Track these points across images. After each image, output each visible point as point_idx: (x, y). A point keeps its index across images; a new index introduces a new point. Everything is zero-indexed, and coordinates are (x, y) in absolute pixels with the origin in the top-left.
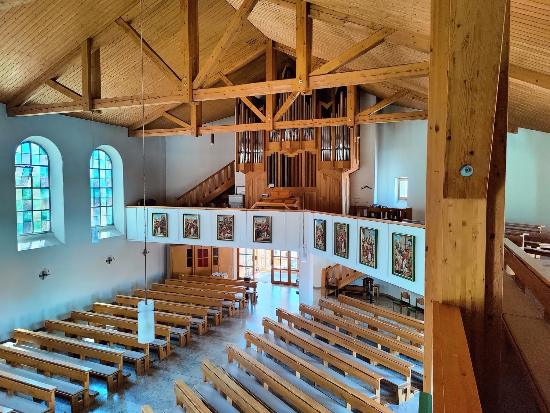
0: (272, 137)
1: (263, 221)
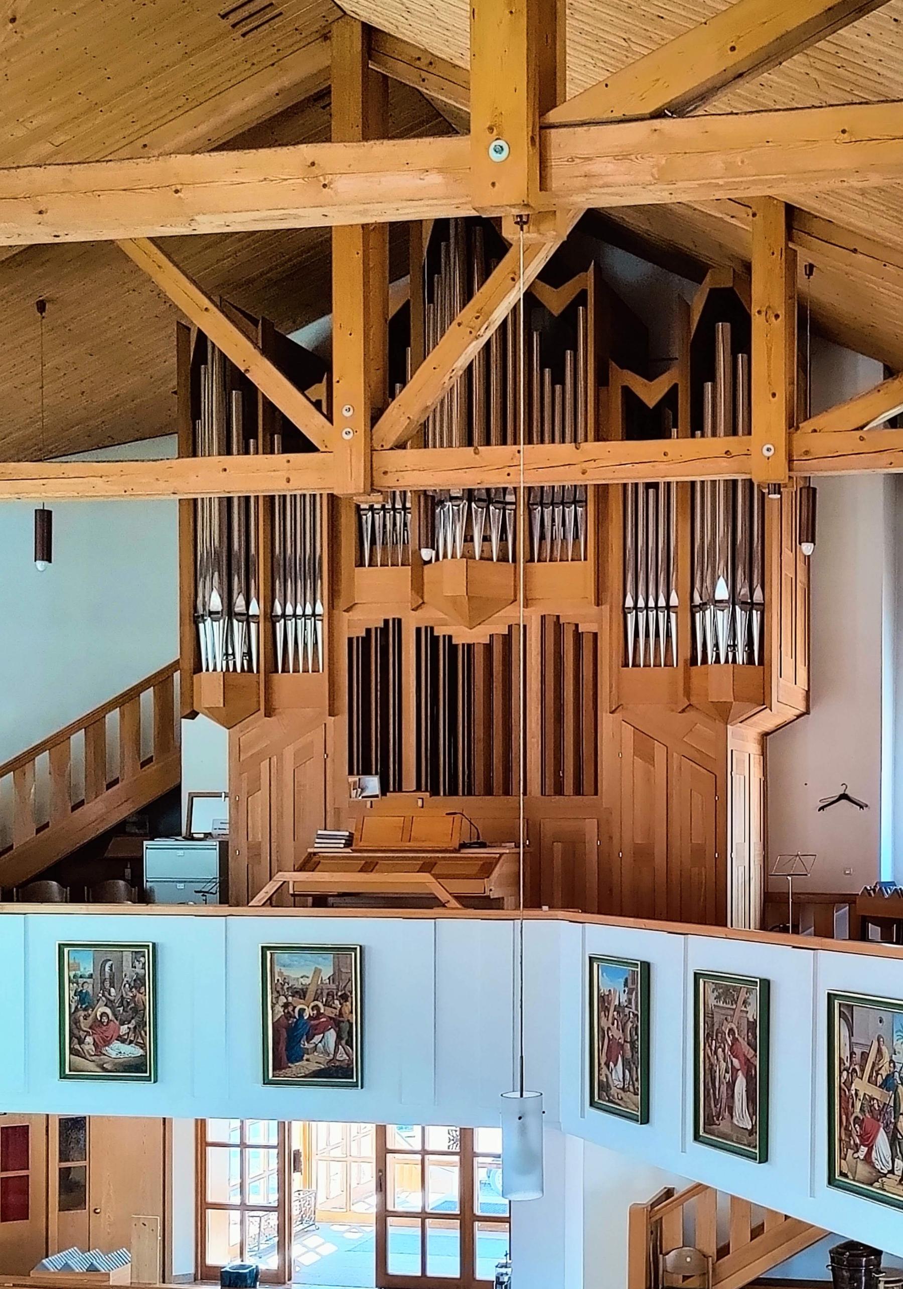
1: (317, 972)
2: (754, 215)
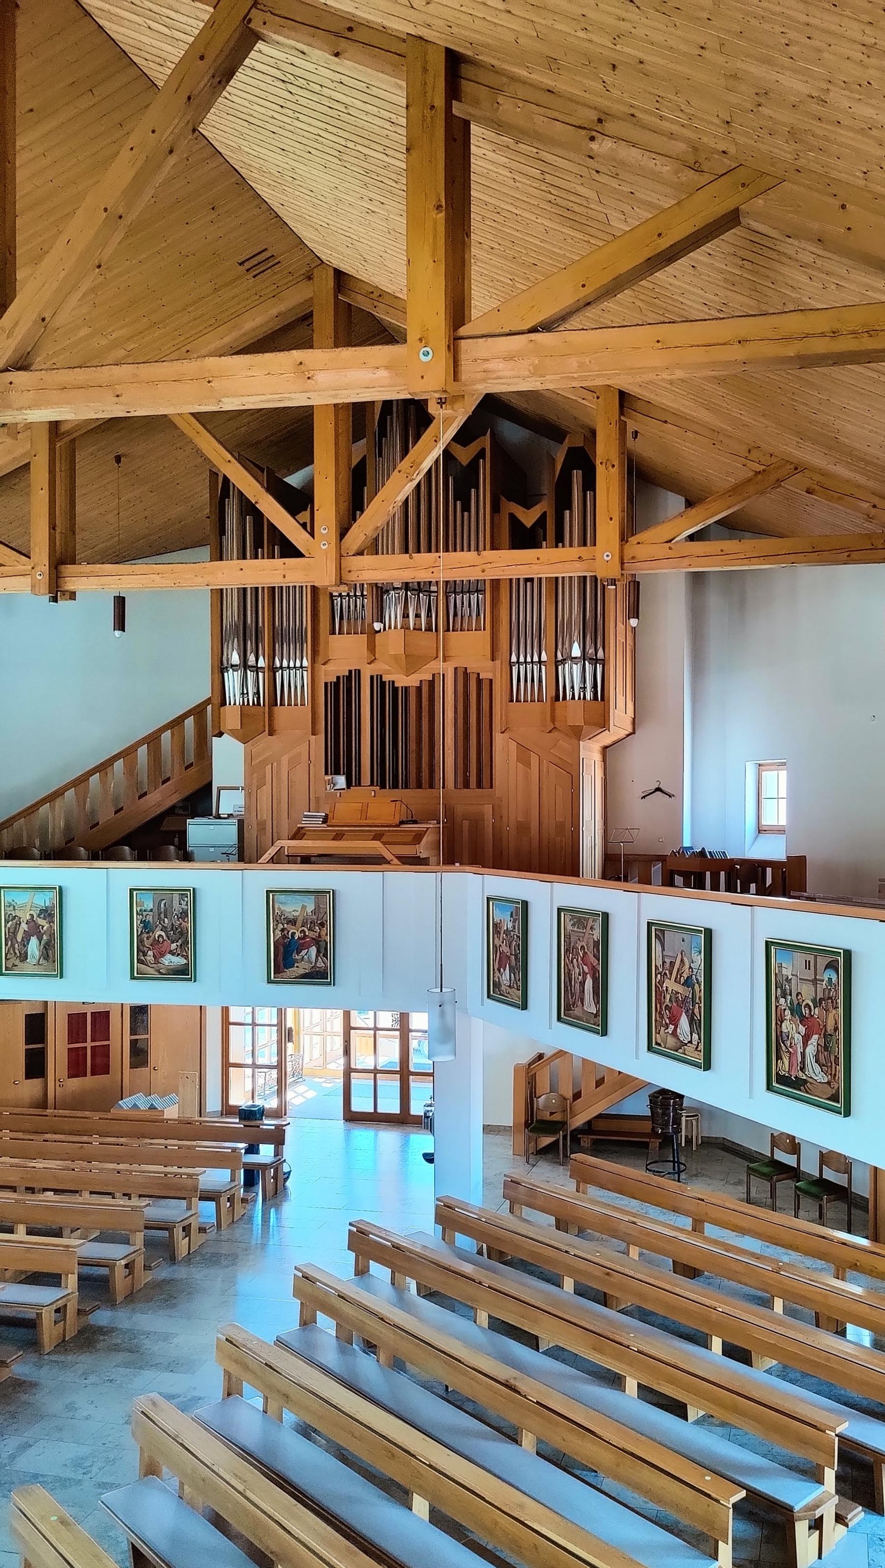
0: (341, 618)
1: (304, 907)
2: (598, 398)
